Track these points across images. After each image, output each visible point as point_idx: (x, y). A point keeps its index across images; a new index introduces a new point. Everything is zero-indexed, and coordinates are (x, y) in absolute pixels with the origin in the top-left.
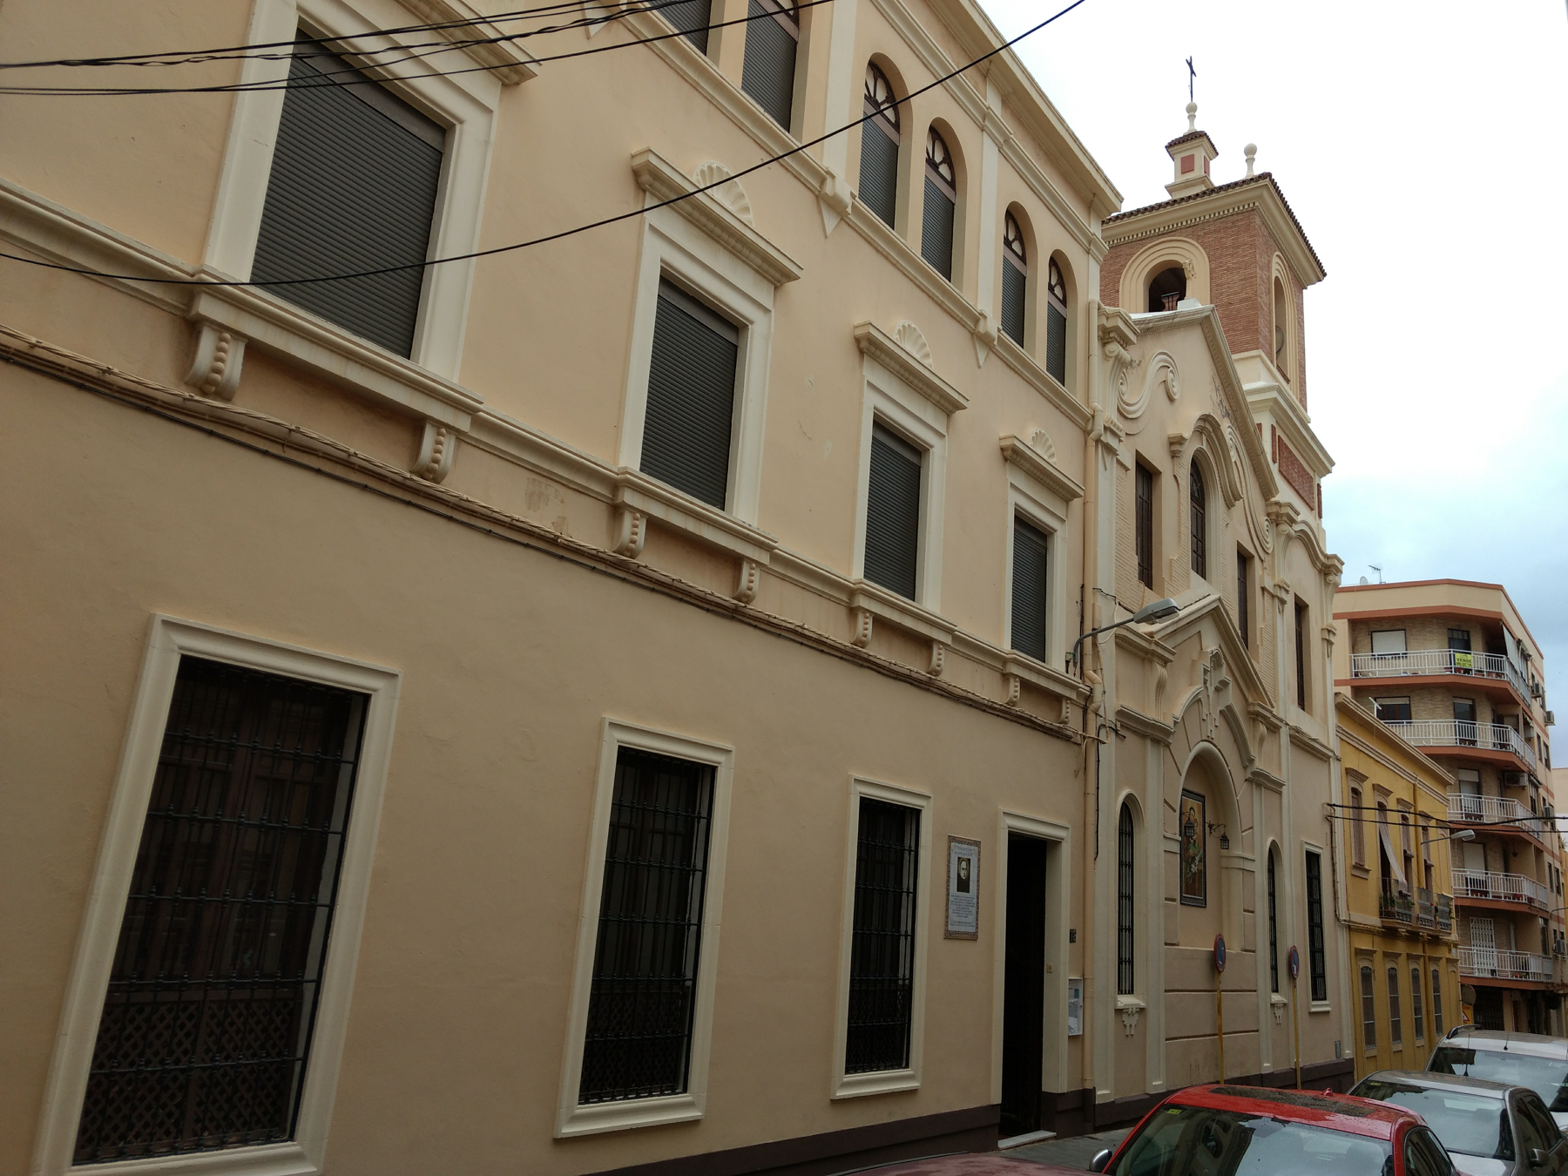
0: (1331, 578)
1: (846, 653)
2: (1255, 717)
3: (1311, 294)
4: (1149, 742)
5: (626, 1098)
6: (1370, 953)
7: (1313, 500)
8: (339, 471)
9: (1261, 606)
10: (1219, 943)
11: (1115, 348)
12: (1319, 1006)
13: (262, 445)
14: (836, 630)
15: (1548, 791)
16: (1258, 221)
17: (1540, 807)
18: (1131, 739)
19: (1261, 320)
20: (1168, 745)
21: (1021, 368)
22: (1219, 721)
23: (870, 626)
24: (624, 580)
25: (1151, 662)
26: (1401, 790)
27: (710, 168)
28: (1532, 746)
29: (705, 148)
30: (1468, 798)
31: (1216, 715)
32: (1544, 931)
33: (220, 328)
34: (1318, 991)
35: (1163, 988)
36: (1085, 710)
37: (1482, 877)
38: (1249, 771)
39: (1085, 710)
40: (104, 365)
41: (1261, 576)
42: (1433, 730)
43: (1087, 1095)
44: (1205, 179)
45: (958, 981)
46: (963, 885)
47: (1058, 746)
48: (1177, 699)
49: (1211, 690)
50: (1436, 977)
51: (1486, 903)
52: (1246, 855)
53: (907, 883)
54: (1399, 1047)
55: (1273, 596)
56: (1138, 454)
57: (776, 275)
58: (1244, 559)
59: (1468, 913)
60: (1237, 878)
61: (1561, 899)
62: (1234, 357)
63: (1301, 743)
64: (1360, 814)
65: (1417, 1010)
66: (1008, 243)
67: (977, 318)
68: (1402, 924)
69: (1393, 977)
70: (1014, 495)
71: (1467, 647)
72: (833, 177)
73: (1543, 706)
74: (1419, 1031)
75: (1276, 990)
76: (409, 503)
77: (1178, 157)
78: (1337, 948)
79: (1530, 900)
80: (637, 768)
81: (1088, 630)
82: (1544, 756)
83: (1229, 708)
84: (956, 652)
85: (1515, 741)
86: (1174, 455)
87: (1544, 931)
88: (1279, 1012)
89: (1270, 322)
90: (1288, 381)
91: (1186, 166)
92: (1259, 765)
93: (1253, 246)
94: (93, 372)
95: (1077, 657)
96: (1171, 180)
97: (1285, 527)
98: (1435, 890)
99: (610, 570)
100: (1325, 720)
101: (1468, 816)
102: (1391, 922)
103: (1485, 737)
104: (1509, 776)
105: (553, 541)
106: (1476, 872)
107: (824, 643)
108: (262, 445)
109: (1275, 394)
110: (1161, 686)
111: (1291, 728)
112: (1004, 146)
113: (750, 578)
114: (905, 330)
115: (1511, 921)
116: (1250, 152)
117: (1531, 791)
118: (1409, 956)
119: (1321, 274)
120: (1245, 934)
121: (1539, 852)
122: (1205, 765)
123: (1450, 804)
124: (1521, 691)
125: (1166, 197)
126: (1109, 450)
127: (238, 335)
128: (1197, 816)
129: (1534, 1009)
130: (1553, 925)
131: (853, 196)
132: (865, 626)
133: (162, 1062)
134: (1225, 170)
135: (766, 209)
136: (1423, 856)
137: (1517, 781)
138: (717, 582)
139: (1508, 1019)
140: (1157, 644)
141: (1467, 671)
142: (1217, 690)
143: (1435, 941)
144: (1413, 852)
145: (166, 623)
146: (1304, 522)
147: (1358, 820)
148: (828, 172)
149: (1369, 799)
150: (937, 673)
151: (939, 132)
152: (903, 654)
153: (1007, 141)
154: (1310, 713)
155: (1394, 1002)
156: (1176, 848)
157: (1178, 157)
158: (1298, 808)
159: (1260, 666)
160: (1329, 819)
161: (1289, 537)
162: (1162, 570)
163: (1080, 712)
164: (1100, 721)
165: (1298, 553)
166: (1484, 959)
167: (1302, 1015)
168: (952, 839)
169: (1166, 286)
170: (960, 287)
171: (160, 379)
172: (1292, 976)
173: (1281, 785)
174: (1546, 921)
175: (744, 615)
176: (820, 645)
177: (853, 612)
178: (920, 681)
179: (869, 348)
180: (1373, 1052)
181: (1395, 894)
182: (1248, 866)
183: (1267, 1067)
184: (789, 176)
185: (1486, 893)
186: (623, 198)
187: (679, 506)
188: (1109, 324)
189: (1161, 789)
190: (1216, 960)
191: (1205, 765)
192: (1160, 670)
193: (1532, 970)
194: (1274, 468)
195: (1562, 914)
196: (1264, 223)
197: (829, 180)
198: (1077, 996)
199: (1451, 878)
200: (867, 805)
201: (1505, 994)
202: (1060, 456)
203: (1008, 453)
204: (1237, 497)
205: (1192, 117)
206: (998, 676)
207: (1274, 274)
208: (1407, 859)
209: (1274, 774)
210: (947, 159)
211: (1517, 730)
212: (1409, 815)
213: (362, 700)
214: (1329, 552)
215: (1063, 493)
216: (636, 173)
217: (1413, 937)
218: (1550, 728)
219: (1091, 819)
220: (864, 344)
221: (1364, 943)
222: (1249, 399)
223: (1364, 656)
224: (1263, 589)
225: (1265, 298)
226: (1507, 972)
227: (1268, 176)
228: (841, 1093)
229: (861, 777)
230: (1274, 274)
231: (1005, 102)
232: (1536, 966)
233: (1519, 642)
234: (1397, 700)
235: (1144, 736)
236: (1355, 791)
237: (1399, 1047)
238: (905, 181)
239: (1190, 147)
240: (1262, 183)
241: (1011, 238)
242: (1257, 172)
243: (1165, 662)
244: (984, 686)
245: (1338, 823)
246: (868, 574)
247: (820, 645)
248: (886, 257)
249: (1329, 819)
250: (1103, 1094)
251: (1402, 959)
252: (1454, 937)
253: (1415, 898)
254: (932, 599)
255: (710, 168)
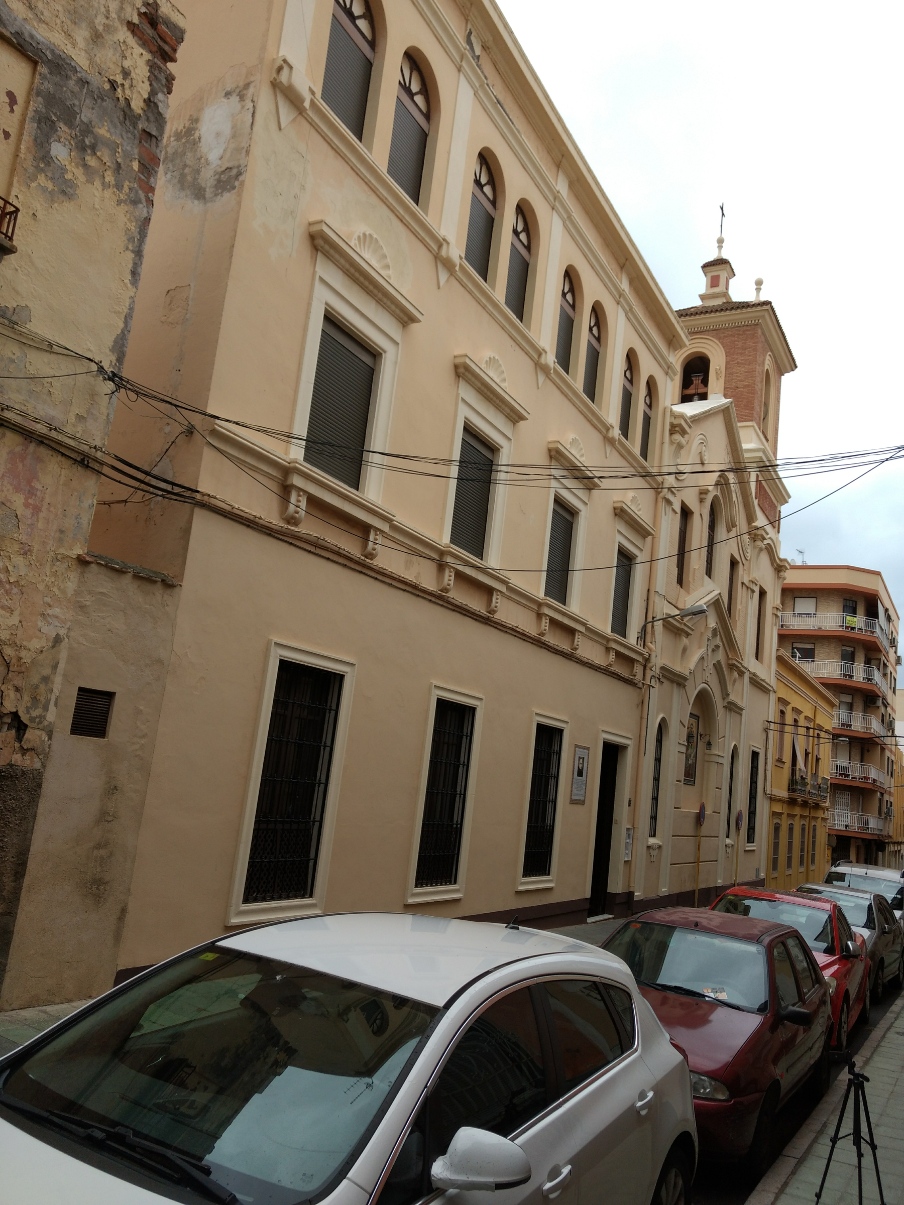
0: (782, 574)
1: (535, 640)
2: (732, 667)
3: (786, 379)
4: (675, 685)
5: (431, 885)
6: (781, 814)
7: (775, 521)
8: (335, 558)
9: (740, 593)
10: (702, 808)
11: (677, 437)
12: (750, 847)
13: (308, 547)
14: (429, 582)
15: (892, 709)
16: (760, 332)
17: (887, 719)
18: (666, 683)
19: (756, 401)
20: (684, 686)
21: (566, 391)
22: (713, 671)
23: (452, 578)
24: (442, 606)
25: (680, 635)
26: (808, 712)
27: (364, 235)
28: (886, 680)
29: (359, 219)
30: (843, 714)
31: (711, 667)
32: (881, 800)
33: (300, 489)
34: (750, 839)
35: (671, 834)
36: (645, 667)
37: (846, 765)
38: (726, 701)
39: (645, 667)
40: (258, 515)
41: (743, 575)
42: (826, 667)
43: (631, 894)
44: (726, 294)
45: (573, 826)
46: (580, 773)
47: (630, 689)
48: (694, 658)
49: (710, 650)
50: (814, 830)
51: (848, 781)
52: (720, 754)
53: (553, 771)
54: (789, 872)
55: (748, 588)
56: (683, 502)
57: (406, 318)
58: (734, 563)
59: (837, 788)
60: (714, 767)
61: (892, 780)
62: (739, 424)
63: (757, 684)
64: (783, 728)
65: (802, 850)
66: (477, 182)
67: (441, 243)
68: (801, 798)
69: (791, 829)
70: (617, 536)
71: (854, 612)
72: (448, 243)
73: (896, 652)
74: (802, 863)
75: (728, 837)
76: (361, 572)
77: (710, 275)
78: (763, 809)
79: (874, 781)
80: (290, 673)
81: (650, 619)
82: (893, 686)
83: (719, 662)
84: (509, 598)
85: (877, 676)
86: (702, 501)
87: (881, 800)
88: (729, 850)
89: (761, 402)
90: (767, 440)
91: (714, 282)
92: (732, 698)
93: (755, 350)
94: (252, 518)
95: (643, 635)
96: (703, 290)
97: (759, 543)
98: (820, 775)
99: (437, 601)
100: (770, 668)
101: (843, 725)
102: (794, 795)
103: (859, 673)
104: (870, 700)
105: (415, 587)
106: (843, 762)
107: (525, 635)
108: (308, 547)
109: (760, 454)
110: (684, 650)
111: (751, 673)
112: (630, 313)
113: (579, 640)
114: (491, 361)
115: (861, 794)
116: (759, 283)
117: (882, 710)
118: (801, 816)
119: (793, 366)
120: (716, 803)
121: (883, 749)
122: (703, 698)
123: (830, 719)
124: (886, 643)
125: (698, 303)
126: (669, 502)
127: (305, 492)
128: (694, 730)
129: (872, 850)
130: (886, 797)
131: (461, 258)
132: (449, 578)
133: (261, 858)
134: (740, 290)
135: (512, 378)
136: (816, 753)
137: (875, 703)
138: (350, 541)
139: (853, 856)
140: (685, 624)
141: (853, 628)
142: (713, 650)
143: (817, 806)
144: (810, 750)
145: (276, 643)
146: (770, 538)
147: (782, 732)
148: (444, 240)
149: (789, 719)
150: (576, 649)
151: (523, 210)
152: (470, 596)
153: (631, 309)
154: (762, 663)
155: (790, 844)
156: (684, 749)
157: (710, 275)
158: (749, 725)
159: (737, 634)
160: (766, 730)
161: (761, 549)
162: (689, 577)
163: (642, 668)
164: (652, 673)
165: (764, 558)
166: (842, 818)
167: (741, 852)
168: (577, 746)
169: (695, 373)
170: (600, 408)
171: (270, 515)
172: (738, 828)
173: (742, 709)
174: (882, 794)
175: (492, 621)
176: (523, 636)
177: (539, 616)
178: (567, 654)
179: (462, 372)
180: (775, 875)
181: (798, 777)
182: (720, 760)
183: (664, 891)
184: (523, 353)
185: (848, 776)
186: (543, 460)
187: (329, 487)
188: (676, 422)
189: (678, 710)
190: (699, 818)
191: (703, 698)
192: (685, 641)
193: (871, 826)
194: (756, 502)
195: (892, 790)
196: (763, 333)
197: (544, 355)
198: (629, 838)
199: (830, 764)
200: (441, 703)
201: (853, 841)
202: (642, 511)
203: (618, 511)
204: (734, 525)
205: (720, 247)
206: (603, 648)
207: (767, 367)
208: (807, 754)
209: (739, 703)
210: (526, 229)
211: (879, 669)
212: (814, 731)
213: (472, 710)
214: (782, 557)
215: (642, 532)
216: (456, 367)
217: (805, 804)
218: (898, 667)
219: (644, 733)
220: (553, 453)
221: (778, 808)
222: (746, 455)
223: (788, 614)
224: (743, 583)
225: (760, 385)
226: (855, 826)
227: (768, 303)
228: (521, 888)
229: (538, 712)
230: (767, 367)
231: (571, 186)
232: (873, 823)
233: (886, 610)
234: (802, 644)
235: (672, 681)
236: (782, 712)
237: (789, 872)
238: (499, 249)
239: (717, 268)
240: (765, 307)
241: (520, 229)
242: (763, 298)
243: (688, 635)
244: (523, 620)
245: (771, 733)
246: (453, 540)
247: (523, 636)
248: (566, 396)
249: (766, 730)
250: (638, 895)
251: (797, 818)
252: (827, 804)
253: (809, 780)
254: (576, 605)
255: (364, 235)
